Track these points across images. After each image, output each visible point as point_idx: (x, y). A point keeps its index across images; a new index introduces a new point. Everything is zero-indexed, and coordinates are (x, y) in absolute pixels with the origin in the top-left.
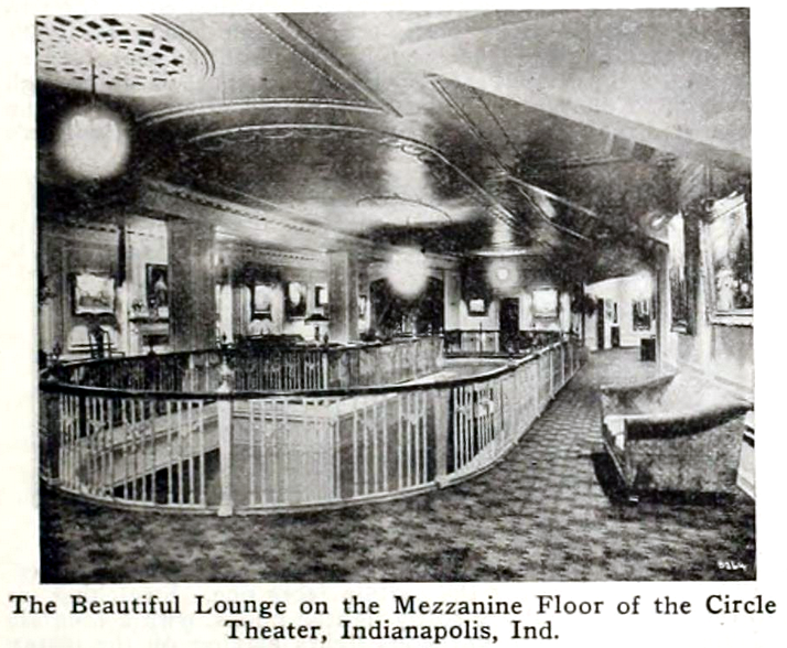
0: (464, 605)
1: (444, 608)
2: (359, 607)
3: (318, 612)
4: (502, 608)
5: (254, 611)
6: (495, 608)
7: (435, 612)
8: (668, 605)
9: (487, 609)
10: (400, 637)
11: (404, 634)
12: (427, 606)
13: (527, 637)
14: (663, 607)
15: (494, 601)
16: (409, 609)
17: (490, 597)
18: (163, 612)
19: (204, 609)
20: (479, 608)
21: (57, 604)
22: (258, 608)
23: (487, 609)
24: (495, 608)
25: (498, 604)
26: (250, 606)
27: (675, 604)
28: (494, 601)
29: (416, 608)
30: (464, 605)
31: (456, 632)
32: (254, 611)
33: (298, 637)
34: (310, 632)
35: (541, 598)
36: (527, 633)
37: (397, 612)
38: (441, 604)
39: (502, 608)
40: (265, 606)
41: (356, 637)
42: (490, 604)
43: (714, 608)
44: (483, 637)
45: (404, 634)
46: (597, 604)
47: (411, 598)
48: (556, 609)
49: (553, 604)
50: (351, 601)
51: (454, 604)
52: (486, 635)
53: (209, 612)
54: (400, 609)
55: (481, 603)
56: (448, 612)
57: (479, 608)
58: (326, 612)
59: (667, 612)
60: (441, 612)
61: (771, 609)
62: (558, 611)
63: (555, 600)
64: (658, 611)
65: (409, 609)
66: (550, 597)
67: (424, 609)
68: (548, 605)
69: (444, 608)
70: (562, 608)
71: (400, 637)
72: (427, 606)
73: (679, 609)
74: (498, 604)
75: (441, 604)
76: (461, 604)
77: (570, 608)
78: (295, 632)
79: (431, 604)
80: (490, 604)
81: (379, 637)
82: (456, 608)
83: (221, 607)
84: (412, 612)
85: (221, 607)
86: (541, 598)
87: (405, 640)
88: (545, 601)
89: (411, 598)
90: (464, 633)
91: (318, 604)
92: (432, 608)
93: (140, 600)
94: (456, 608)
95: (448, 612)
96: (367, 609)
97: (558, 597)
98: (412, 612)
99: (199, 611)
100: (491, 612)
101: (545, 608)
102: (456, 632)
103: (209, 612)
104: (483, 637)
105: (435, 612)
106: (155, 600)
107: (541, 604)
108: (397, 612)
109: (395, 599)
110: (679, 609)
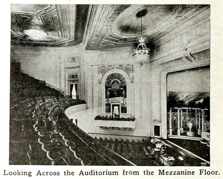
0: (178, 172)
1: (173, 173)
2: (69, 173)
3: (134, 174)
4: (189, 173)
5: (27, 175)
6: (23, 174)
7: (170, 174)
8: (147, 172)
9: (185, 173)
10: (179, 174)
11: (180, 173)
12: (168, 173)
13: (24, 175)
14: (146, 173)
15: (187, 171)
16: (163, 174)
17: (107, 170)
18: (26, 172)
19: (5, 174)
20: (183, 173)
21: (195, 172)
22: (28, 174)
23: (185, 173)
24: (23, 174)
25: (24, 172)
26: (26, 173)
27: (149, 172)
28: (187, 171)
29: (165, 173)
30: (178, 172)
31: (15, 173)
32: (27, 175)
33: (151, 174)
34: (46, 174)
35: (201, 170)
36: (94, 174)
37: (159, 174)
38: (172, 172)
39: (189, 173)
40: (30, 173)
41: (188, 174)
42: (186, 172)
43: (44, 174)
44: (57, 175)
45: (180, 173)
46: (216, 172)
47: (163, 170)
48: (205, 173)
49: (204, 172)
50: (66, 172)
51: (175, 172)
52: (58, 174)
53: (7, 175)
54: (160, 174)
55: (183, 172)
56: (174, 174)
57: (183, 173)
58: (138, 174)
59: (68, 175)
60: (172, 174)
61: (193, 173)
62: (205, 174)
63: (205, 171)
64: (65, 175)
65: (163, 174)
66: (203, 170)
67: (167, 174)
68: (202, 172)
69: (173, 173)
70: (206, 173)
71: (179, 174)
72: (168, 173)
73: (191, 173)
74: (24, 172)
75: (172, 172)
76: (178, 172)
77: (209, 173)
78: (98, 173)
79: (169, 172)
80: (186, 172)
81: (92, 175)
82: (176, 173)
83: (11, 173)
84: (164, 174)
85: (11, 173)
86: (201, 170)
87: (181, 175)
88: (202, 171)
89: (163, 170)
90: (17, 174)
91: (88, 175)
92: (169, 173)
93: (185, 171)
94: (176, 173)
95: (174, 174)
96: (150, 174)
97: (205, 170)
98: (164, 174)
99: (5, 175)
100: (186, 174)
101: (202, 173)
102: (15, 173)
103: (7, 175)
104: (57, 175)
105: (170, 174)
106: (124, 171)
107: (201, 172)
108: (159, 174)
109: (159, 171)
110: (71, 174)
